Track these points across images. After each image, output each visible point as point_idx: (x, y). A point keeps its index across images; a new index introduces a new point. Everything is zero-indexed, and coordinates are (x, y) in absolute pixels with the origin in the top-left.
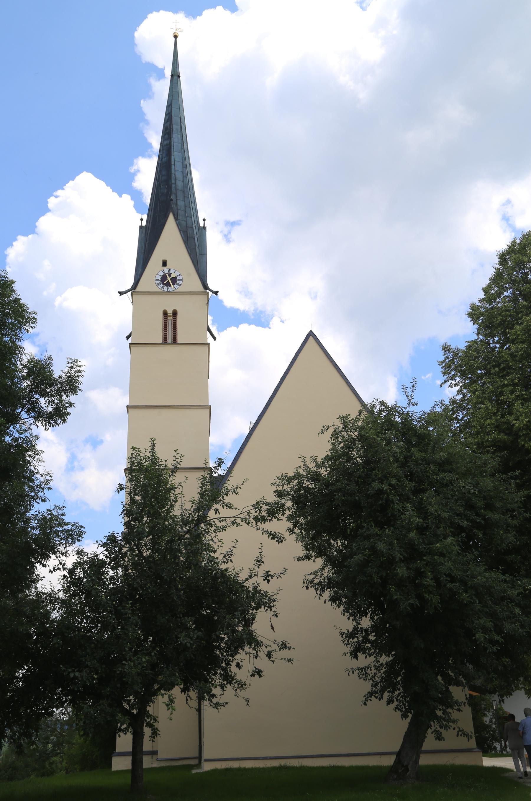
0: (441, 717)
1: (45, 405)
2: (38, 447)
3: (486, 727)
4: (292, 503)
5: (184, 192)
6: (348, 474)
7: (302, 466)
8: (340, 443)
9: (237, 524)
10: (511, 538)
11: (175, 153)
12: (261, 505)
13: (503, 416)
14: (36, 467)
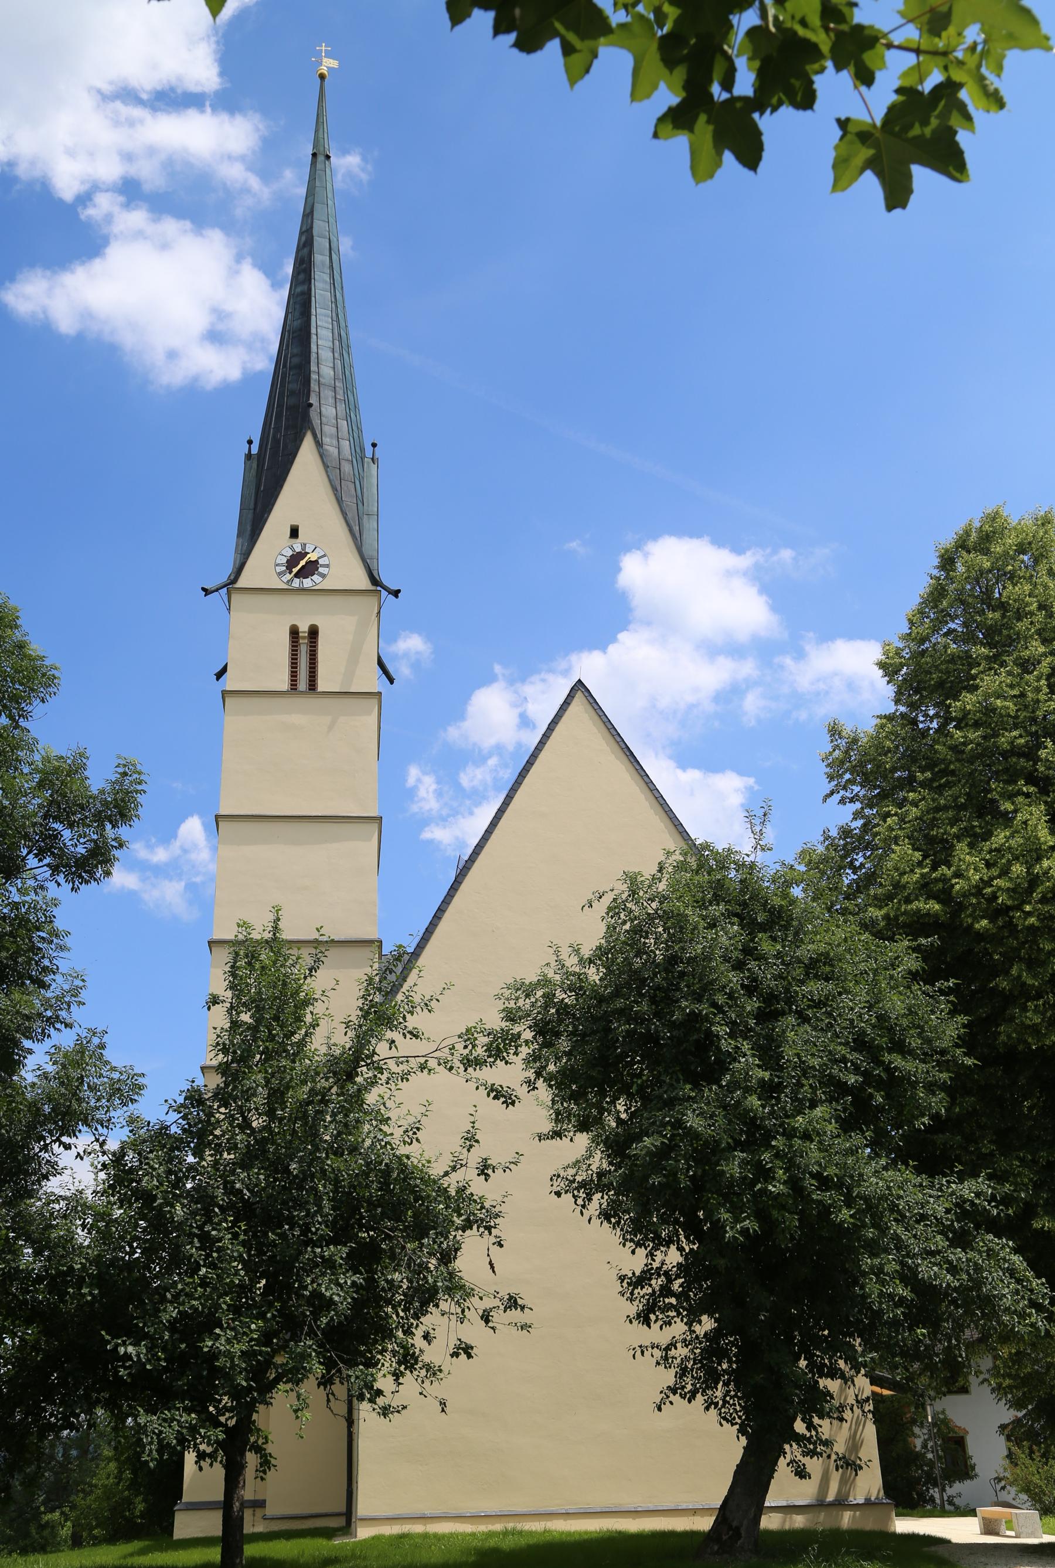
0: (803, 1436)
1: (71, 842)
2: (59, 924)
3: (916, 1458)
4: (533, 1033)
6: (637, 979)
7: (553, 964)
8: (624, 922)
9: (430, 1070)
10: (938, 1103)
12: (476, 1035)
13: (934, 868)
14: (55, 961)
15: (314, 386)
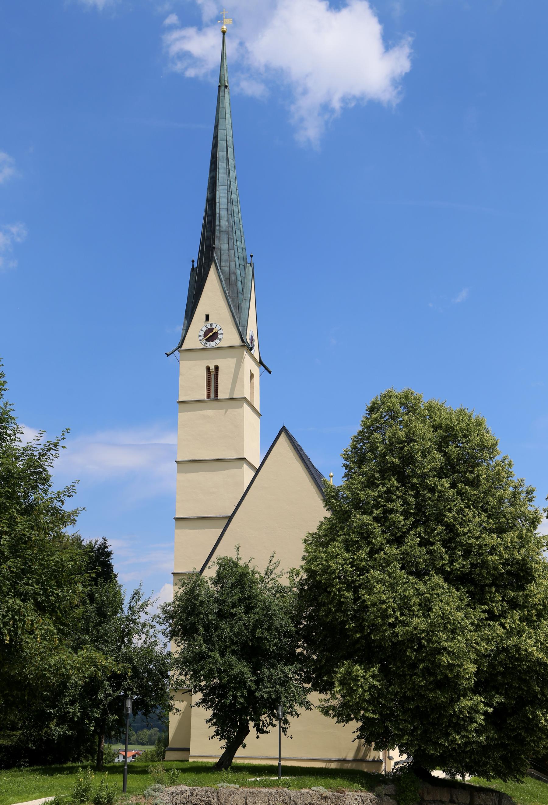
5: (228, 233)
11: (221, 187)
15: (217, 234)
